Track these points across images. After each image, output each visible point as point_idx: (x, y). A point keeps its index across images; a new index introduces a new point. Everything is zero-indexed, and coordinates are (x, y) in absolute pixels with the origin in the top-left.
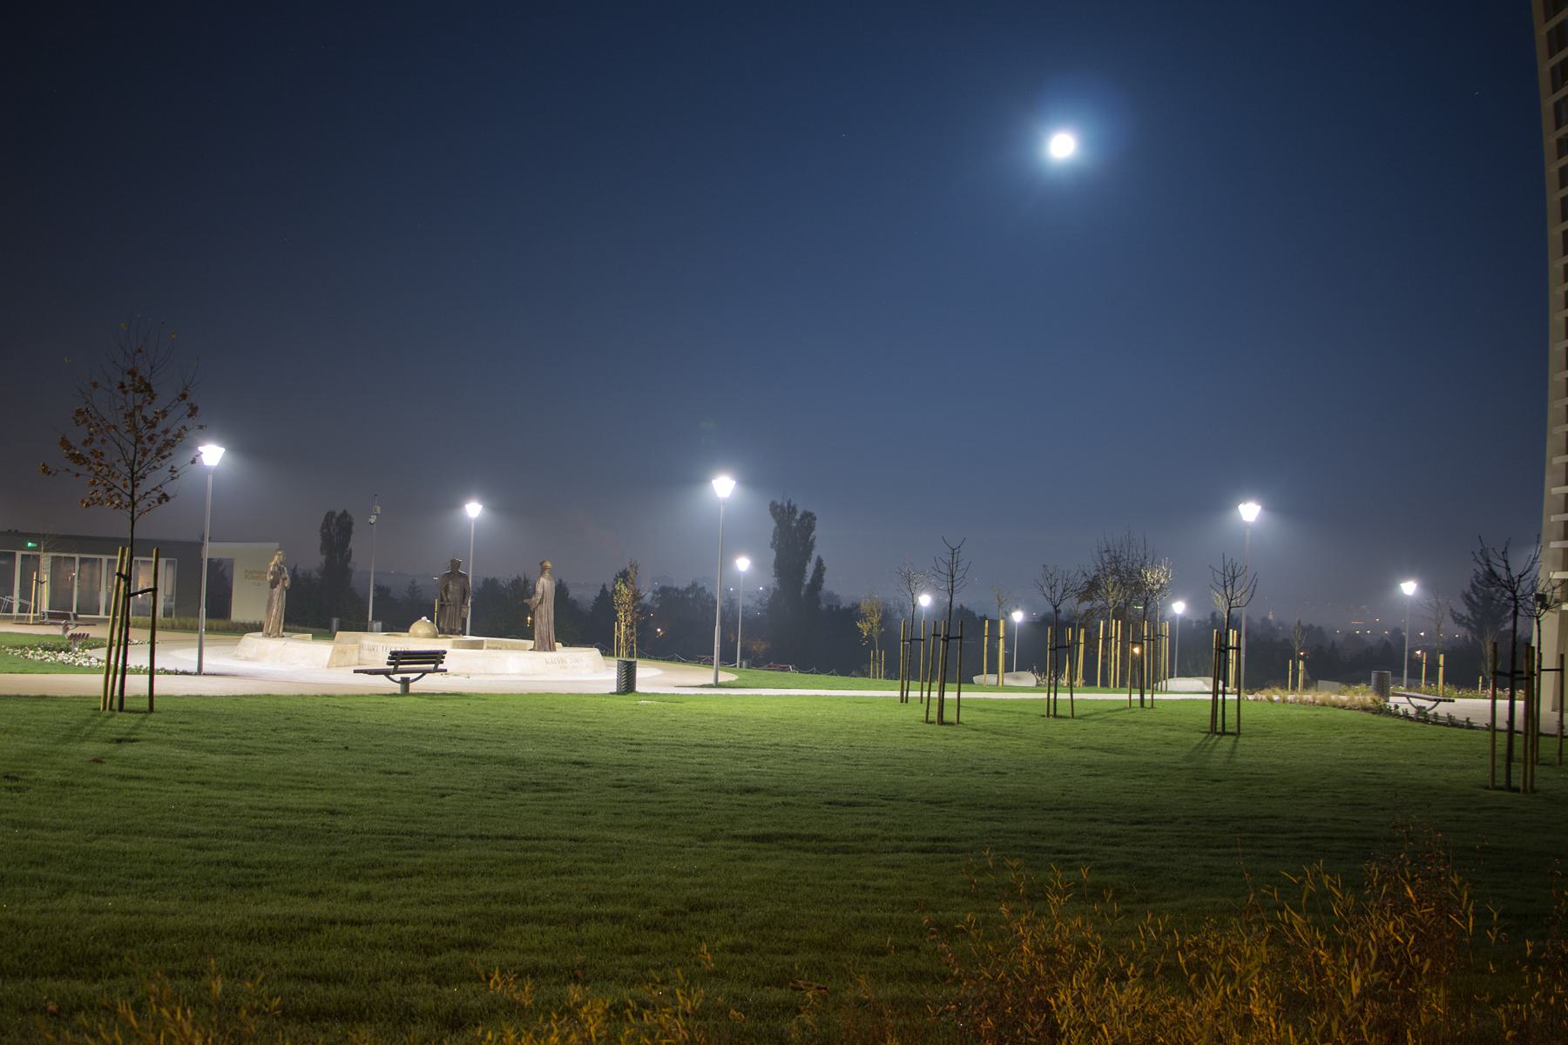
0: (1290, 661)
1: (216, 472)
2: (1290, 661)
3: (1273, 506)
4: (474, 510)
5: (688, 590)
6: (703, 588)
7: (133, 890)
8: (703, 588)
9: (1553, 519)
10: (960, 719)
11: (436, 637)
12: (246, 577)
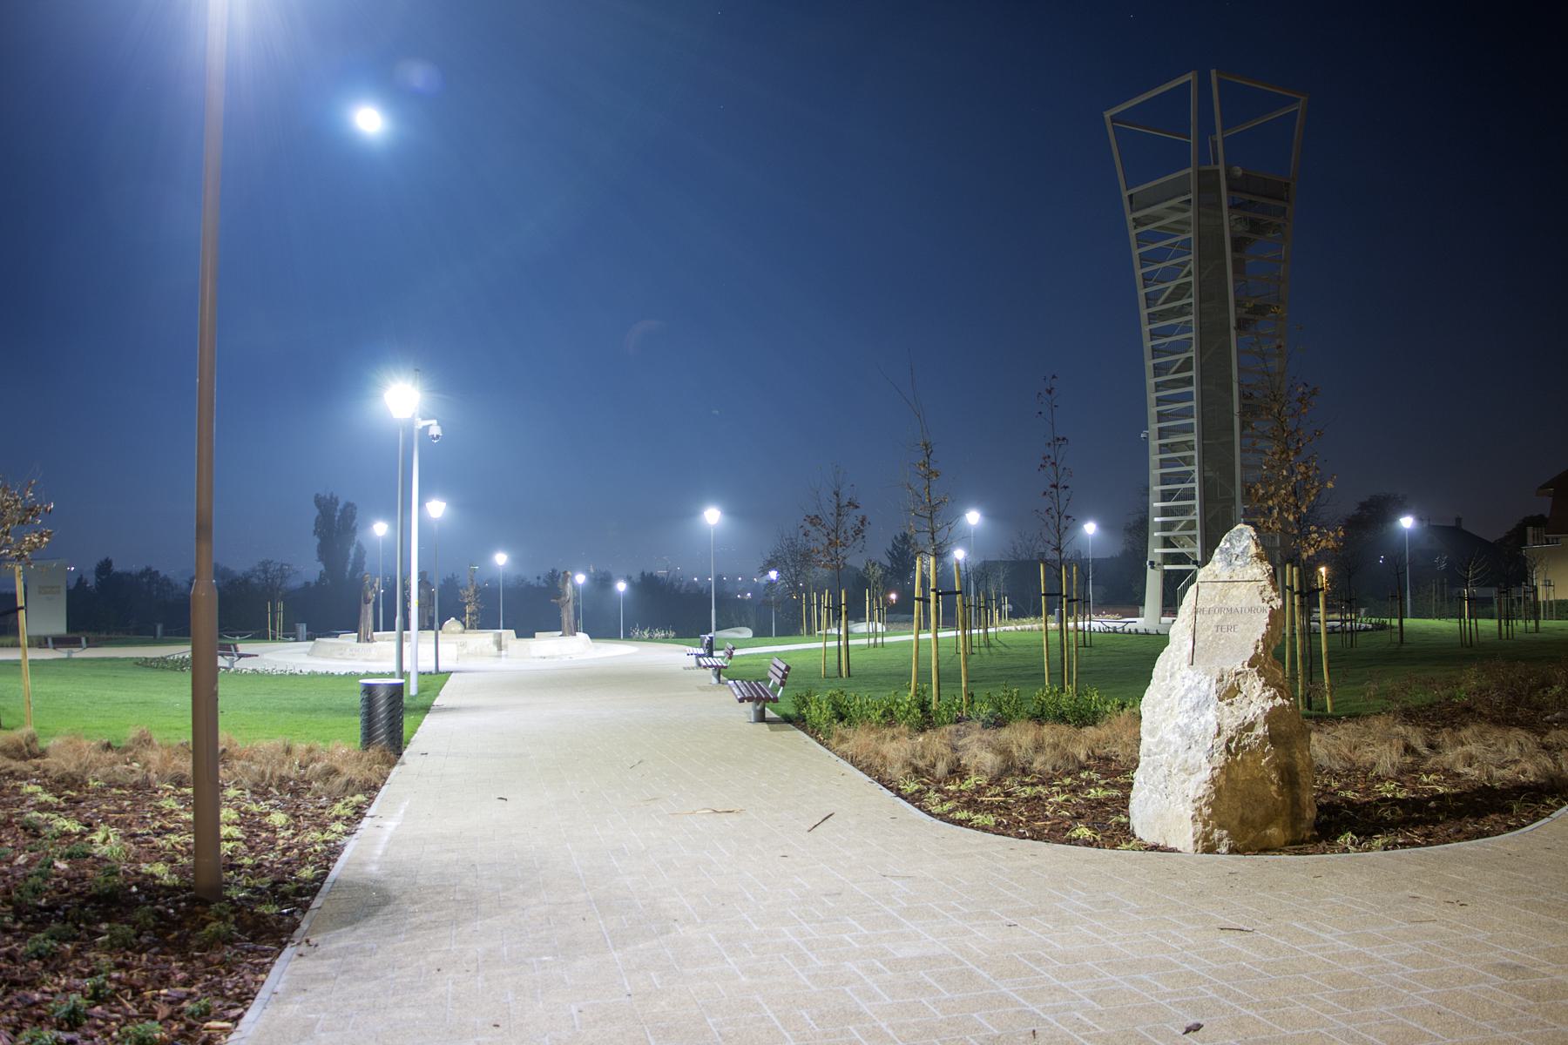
0: (269, 604)
1: (1411, 532)
2: (269, 604)
3: (731, 511)
4: (712, 516)
5: (143, 574)
6: (157, 572)
7: (945, 963)
8: (157, 572)
9: (1156, 534)
10: (440, 665)
11: (463, 633)
12: (40, 592)
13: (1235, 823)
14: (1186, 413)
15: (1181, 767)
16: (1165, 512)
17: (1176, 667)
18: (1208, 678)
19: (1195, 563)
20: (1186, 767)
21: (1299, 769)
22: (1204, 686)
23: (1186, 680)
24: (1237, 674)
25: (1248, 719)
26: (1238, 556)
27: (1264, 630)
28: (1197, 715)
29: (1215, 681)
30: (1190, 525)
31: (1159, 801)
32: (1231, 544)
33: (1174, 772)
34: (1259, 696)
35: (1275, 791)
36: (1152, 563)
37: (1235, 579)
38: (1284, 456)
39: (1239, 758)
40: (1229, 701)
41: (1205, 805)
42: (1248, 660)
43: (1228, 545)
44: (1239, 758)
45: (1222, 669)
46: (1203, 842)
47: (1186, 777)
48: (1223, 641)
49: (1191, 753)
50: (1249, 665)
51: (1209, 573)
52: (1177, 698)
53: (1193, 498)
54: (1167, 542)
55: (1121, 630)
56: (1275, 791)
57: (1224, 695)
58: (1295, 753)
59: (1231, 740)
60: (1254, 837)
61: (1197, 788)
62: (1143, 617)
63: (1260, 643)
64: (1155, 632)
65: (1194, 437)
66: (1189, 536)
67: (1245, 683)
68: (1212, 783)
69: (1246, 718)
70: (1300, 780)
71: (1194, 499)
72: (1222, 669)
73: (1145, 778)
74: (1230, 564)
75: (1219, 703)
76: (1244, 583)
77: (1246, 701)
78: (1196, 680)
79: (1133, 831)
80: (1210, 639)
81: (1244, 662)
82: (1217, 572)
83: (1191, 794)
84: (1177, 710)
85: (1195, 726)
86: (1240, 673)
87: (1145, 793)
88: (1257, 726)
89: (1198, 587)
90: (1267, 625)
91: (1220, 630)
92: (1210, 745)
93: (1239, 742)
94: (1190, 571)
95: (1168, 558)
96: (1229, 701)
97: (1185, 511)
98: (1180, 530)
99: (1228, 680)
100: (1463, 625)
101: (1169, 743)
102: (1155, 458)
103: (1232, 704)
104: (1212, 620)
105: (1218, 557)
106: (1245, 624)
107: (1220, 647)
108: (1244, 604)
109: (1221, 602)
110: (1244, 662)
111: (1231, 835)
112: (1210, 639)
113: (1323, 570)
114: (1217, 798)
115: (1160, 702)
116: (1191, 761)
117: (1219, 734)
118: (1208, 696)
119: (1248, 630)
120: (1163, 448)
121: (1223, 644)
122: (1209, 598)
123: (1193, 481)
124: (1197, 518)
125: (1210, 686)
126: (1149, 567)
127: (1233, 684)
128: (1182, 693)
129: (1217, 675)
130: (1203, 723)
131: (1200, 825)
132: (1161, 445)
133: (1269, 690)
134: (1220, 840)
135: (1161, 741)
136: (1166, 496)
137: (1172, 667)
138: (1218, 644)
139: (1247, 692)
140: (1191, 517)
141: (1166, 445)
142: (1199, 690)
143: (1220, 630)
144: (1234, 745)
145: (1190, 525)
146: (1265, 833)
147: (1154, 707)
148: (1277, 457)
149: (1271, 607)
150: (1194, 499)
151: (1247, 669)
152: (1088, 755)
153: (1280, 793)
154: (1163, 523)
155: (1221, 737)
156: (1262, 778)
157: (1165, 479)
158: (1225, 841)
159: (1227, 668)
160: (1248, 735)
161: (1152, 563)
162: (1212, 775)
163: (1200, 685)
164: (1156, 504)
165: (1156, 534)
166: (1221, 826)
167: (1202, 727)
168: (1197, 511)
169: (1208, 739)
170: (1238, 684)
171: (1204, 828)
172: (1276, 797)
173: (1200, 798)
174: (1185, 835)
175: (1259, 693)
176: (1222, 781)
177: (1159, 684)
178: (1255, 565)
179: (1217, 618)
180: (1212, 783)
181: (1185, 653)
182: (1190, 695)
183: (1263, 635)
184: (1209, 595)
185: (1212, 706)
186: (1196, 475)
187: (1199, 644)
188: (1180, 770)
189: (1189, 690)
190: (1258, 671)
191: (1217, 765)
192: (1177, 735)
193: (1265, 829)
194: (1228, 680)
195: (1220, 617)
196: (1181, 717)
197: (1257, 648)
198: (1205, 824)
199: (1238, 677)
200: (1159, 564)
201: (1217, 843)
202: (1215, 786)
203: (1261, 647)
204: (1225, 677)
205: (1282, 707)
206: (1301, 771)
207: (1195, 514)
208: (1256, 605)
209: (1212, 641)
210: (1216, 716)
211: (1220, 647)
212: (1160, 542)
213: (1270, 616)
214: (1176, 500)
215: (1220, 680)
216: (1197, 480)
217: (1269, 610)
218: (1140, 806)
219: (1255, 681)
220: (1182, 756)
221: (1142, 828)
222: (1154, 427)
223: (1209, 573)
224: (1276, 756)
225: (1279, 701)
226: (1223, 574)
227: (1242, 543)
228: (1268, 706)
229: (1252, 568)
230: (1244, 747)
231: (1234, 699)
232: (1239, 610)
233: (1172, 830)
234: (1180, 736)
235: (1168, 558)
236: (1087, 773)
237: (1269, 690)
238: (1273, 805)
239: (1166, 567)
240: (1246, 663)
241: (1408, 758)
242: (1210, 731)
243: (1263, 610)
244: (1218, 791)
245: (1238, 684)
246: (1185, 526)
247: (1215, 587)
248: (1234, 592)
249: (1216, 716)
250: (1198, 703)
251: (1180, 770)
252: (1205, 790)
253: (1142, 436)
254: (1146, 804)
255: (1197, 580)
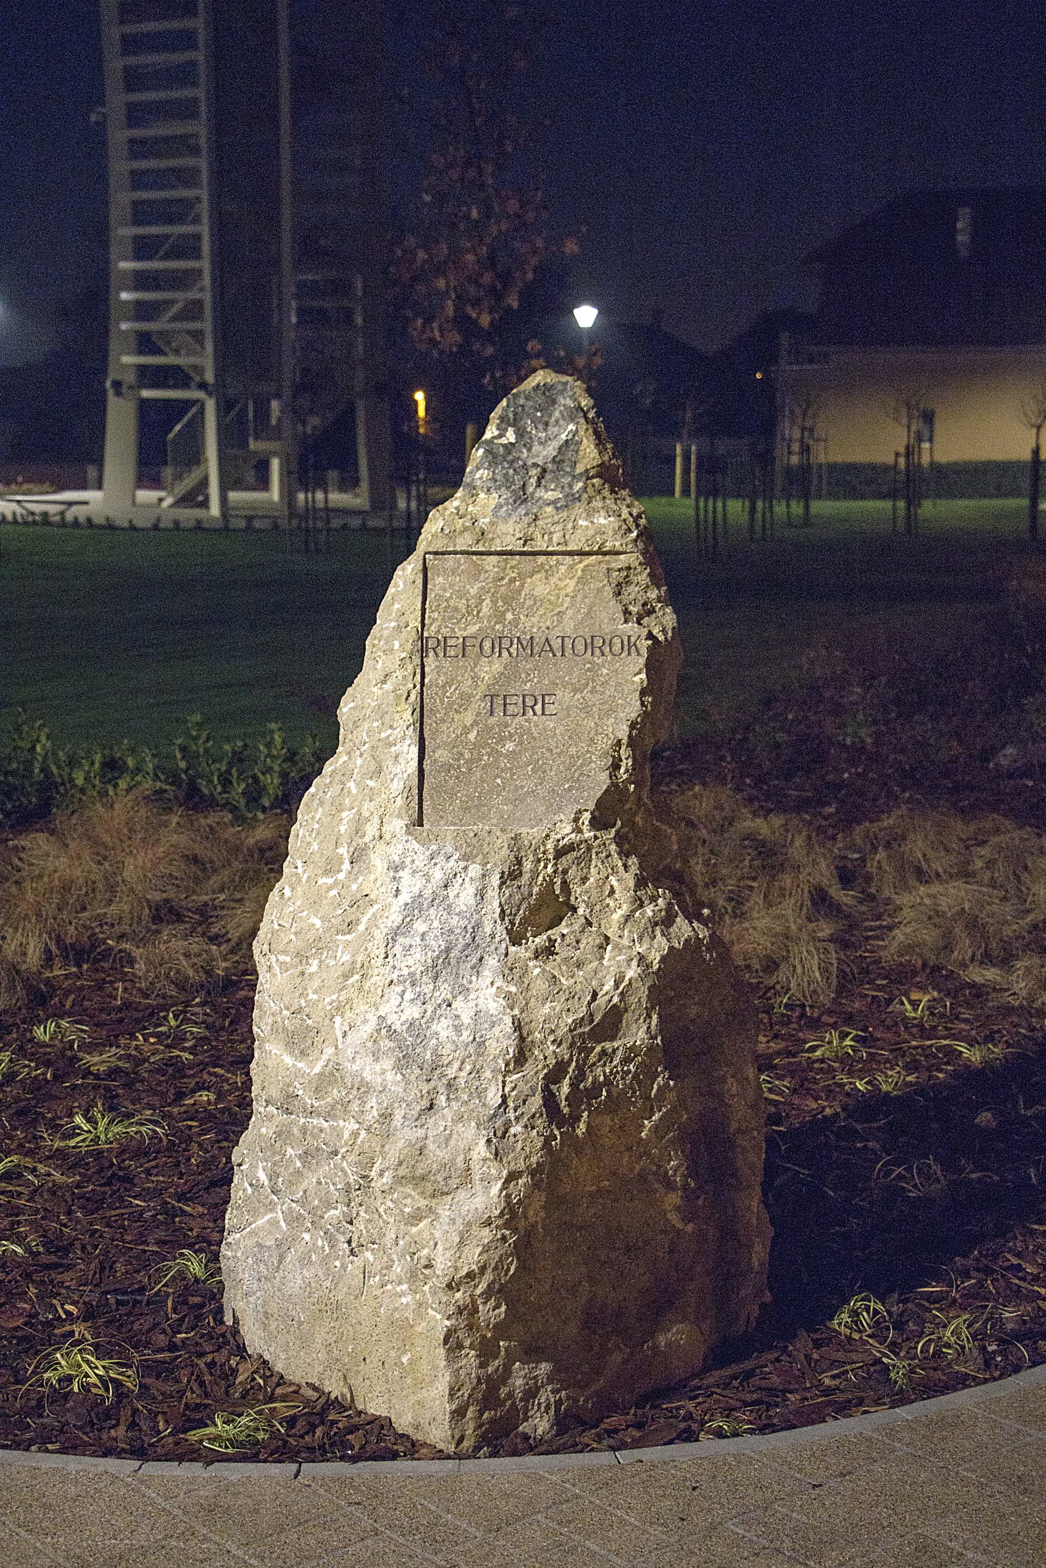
9: (124, 326)
13: (572, 1329)
14: (184, 75)
15: (401, 1172)
16: (141, 281)
17: (371, 830)
18: (475, 870)
19: (203, 386)
20: (419, 1172)
21: (734, 1126)
22: (464, 896)
23: (405, 874)
24: (560, 853)
25: (601, 1001)
26: (544, 471)
27: (632, 709)
28: (444, 991)
29: (495, 880)
30: (193, 311)
31: (325, 1260)
32: (520, 433)
33: (378, 1184)
34: (628, 918)
35: (678, 1208)
36: (117, 385)
37: (541, 545)
38: (472, 173)
39: (582, 1128)
40: (540, 940)
41: (487, 1294)
42: (591, 806)
43: (511, 436)
44: (582, 1128)
45: (516, 838)
46: (481, 1413)
47: (422, 1203)
48: (510, 746)
49: (436, 1125)
50: (596, 823)
51: (459, 523)
52: (379, 935)
53: (195, 253)
54: (145, 343)
55: (57, 518)
56: (678, 1208)
57: (525, 921)
58: (723, 1080)
59: (555, 1075)
60: (625, 1362)
61: (461, 1243)
62: (100, 487)
63: (624, 752)
64: (126, 525)
65: (200, 129)
66: (189, 332)
67: (584, 880)
68: (507, 1225)
69: (595, 996)
70: (739, 1163)
71: (199, 257)
72: (516, 838)
73: (273, 1176)
74: (521, 497)
75: (512, 949)
76: (568, 559)
77: (590, 940)
78: (438, 875)
79: (235, 1331)
80: (472, 736)
81: (580, 812)
82: (484, 522)
83: (442, 1262)
84: (379, 976)
85: (443, 1029)
86: (570, 848)
87: (274, 1223)
88: (628, 1017)
89: (425, 570)
90: (643, 693)
91: (499, 711)
92: (493, 1098)
93: (580, 1076)
94: (189, 404)
95: (150, 376)
96: (540, 940)
97: (182, 280)
98: (174, 319)
99: (535, 874)
100: (702, 512)
101: (364, 1088)
102: (120, 167)
103: (549, 951)
104: (475, 678)
105: (483, 473)
106: (576, 691)
107: (504, 762)
108: (568, 626)
109: (500, 617)
110: (580, 812)
111: (562, 1376)
112: (472, 736)
113: (419, 396)
114: (522, 1267)
115: (319, 946)
116: (436, 1154)
117: (520, 1059)
118: (478, 925)
119: (585, 708)
120: (139, 148)
121: (512, 755)
122: (462, 604)
123: (196, 220)
124: (207, 297)
125: (481, 894)
126: (111, 393)
127: (552, 884)
128: (395, 918)
129: (500, 857)
130: (466, 1018)
131: (470, 1358)
132: (132, 141)
133: (654, 899)
134: (531, 1394)
135: (331, 1077)
136: (143, 249)
137: (358, 831)
138: (494, 753)
139: (590, 906)
140: (193, 295)
141: (143, 142)
142: (449, 909)
143: (499, 711)
144: (565, 1089)
145: (193, 311)
146: (655, 1347)
147: (302, 957)
148: (455, 174)
149: (650, 636)
150: (199, 257)
151: (588, 834)
152: (48, 951)
153: (689, 1214)
154: (138, 303)
155: (529, 1068)
156: (642, 1177)
157: (141, 214)
158: (546, 1395)
159: (532, 833)
160: (604, 1052)
161: (117, 385)
162: (508, 1196)
163: (452, 892)
164: (123, 265)
165: (124, 326)
166: (532, 1352)
167: (466, 1036)
168: (207, 280)
169: (488, 1074)
170: (565, 884)
171: (483, 1365)
172: (680, 1225)
173: (470, 1275)
174: (420, 1384)
175: (625, 909)
176: (535, 1214)
177: (313, 881)
178: (597, 503)
179: (490, 669)
180: (507, 1225)
181: (397, 786)
182: (420, 926)
183: (632, 726)
184: (461, 594)
185: (492, 962)
186: (204, 208)
187: (439, 755)
188: (399, 1180)
189: (415, 908)
190: (619, 840)
191: (521, 1165)
192: (387, 1064)
193: (652, 1334)
194: (535, 874)
195: (497, 667)
196: (395, 1000)
197: (616, 766)
198: (486, 1352)
199: (564, 862)
200: (130, 387)
201: (520, 1405)
202: (515, 1230)
203: (626, 764)
204: (527, 866)
205: (693, 946)
206: (739, 1130)
207: (202, 289)
208: (607, 628)
209: (477, 746)
210: (508, 996)
211: (504, 762)
212: (132, 340)
213: (649, 666)
214: (166, 257)
215: (511, 875)
216: (205, 219)
217: (645, 644)
218: (258, 1261)
219: (614, 870)
220: (405, 1135)
221: (265, 1327)
222: (117, 100)
223: (459, 523)
224: (682, 1103)
225: (683, 928)
226: (502, 528)
227: (553, 430)
228: (656, 949)
229: (590, 514)
230: (596, 1087)
231: (554, 933)
232: (556, 644)
233: (374, 1361)
234: (398, 1067)
235: (150, 376)
236: (52, 1027)
237: (654, 899)
238: (671, 1252)
239: (146, 394)
240: (586, 816)
241: (822, 924)
242: (493, 1048)
243: (629, 646)
244: (523, 1249)
245: (565, 884)
246: (182, 310)
247: (480, 570)
248: (538, 586)
249: (508, 996)
250: (448, 950)
251: (399, 1180)
252: (486, 1249)
253: (93, 118)
254: (281, 1258)
255: (422, 546)
